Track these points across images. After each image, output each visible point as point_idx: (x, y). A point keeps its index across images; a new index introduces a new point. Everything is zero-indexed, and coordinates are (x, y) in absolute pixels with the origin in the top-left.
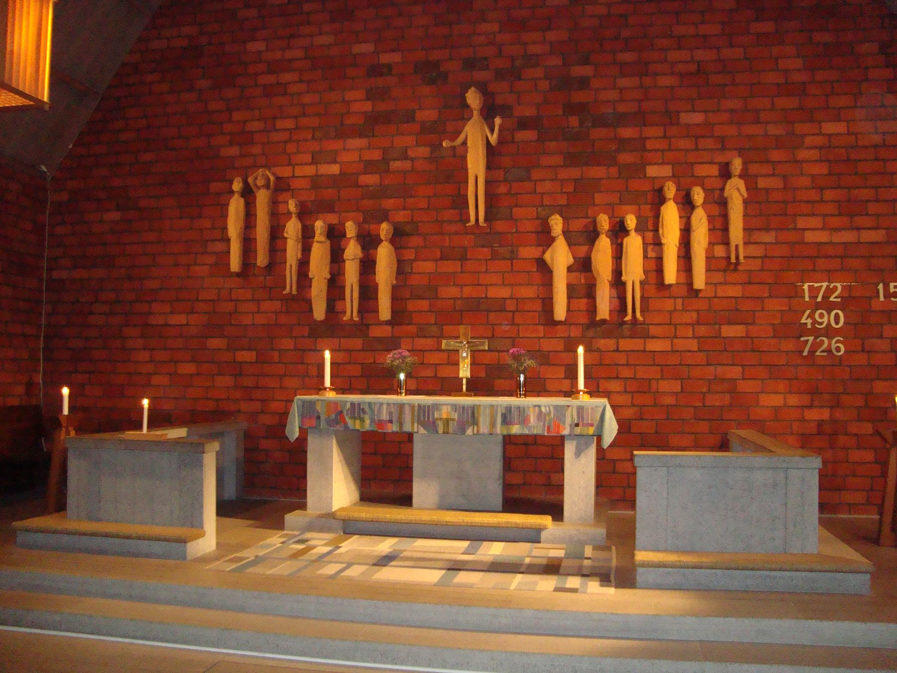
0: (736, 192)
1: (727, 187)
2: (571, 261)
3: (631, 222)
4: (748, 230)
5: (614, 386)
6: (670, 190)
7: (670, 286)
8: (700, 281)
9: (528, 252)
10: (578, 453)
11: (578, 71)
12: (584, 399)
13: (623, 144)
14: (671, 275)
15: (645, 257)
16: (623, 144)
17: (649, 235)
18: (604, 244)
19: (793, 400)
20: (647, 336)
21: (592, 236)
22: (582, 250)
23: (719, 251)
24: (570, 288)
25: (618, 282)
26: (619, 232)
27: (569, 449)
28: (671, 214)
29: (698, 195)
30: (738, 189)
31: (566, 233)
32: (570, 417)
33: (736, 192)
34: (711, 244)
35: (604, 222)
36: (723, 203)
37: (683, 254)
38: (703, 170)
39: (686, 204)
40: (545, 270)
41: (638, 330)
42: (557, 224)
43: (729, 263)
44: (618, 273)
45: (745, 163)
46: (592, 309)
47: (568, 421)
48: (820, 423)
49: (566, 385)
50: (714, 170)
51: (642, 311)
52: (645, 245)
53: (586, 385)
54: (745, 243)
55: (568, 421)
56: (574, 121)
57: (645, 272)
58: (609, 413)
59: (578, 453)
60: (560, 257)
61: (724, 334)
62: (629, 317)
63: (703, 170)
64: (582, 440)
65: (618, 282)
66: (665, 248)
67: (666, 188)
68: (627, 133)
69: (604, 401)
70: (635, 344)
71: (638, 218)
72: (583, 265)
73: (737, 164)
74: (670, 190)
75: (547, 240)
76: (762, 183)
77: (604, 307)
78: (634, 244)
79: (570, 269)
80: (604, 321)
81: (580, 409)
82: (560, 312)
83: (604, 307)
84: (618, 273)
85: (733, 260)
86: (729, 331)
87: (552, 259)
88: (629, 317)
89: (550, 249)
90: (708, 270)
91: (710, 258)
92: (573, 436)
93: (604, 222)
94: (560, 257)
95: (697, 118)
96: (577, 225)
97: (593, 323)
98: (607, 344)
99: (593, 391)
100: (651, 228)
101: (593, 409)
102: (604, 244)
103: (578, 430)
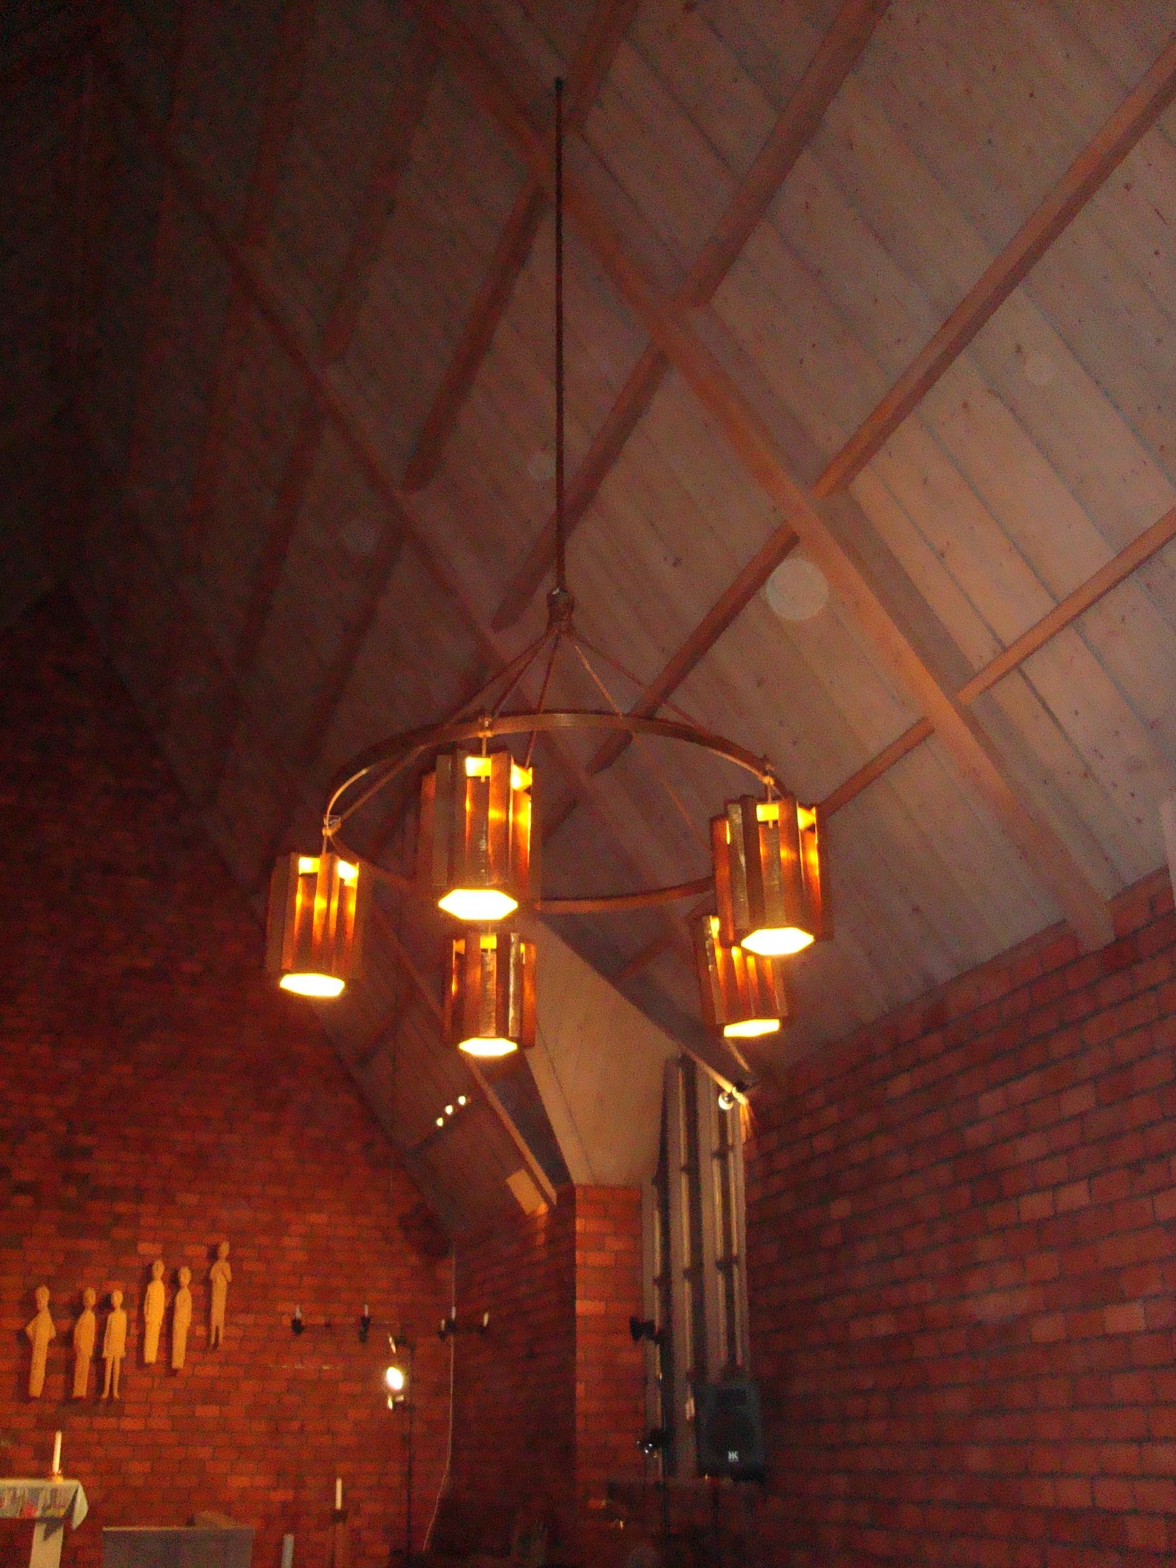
0: (221, 1275)
1: (213, 1270)
2: (54, 1334)
3: (118, 1298)
4: (228, 1311)
5: (81, 1467)
6: (159, 1269)
7: (150, 1364)
8: (178, 1361)
9: (12, 1323)
10: (47, 1535)
11: (84, 1140)
12: (59, 1481)
13: (118, 1219)
14: (151, 1353)
15: (128, 1334)
16: (118, 1219)
17: (135, 1313)
18: (89, 1319)
19: (260, 1481)
20: (120, 1414)
21: (77, 1309)
22: (65, 1324)
23: (200, 1331)
24: (49, 1363)
25: (99, 1361)
26: (104, 1307)
27: (39, 1532)
28: (157, 1293)
29: (185, 1276)
30: (223, 1273)
31: (51, 1305)
32: (44, 1498)
33: (221, 1275)
34: (193, 1323)
35: (91, 1297)
36: (208, 1283)
37: (164, 1331)
38: (191, 1250)
39: (173, 1284)
40: (26, 1344)
41: (115, 1408)
42: (43, 1296)
43: (208, 1344)
44: (99, 1346)
45: (232, 1248)
46: (70, 1384)
47: (40, 1504)
48: (285, 1505)
49: (33, 1465)
50: (203, 1251)
51: (119, 1389)
52: (129, 1322)
53: (61, 1466)
54: (226, 1325)
55: (40, 1504)
56: (71, 1192)
57: (126, 1348)
58: (81, 1490)
59: (47, 1535)
60: (43, 1329)
61: (197, 1414)
62: (105, 1395)
63: (191, 1250)
64: (52, 1524)
65: (99, 1361)
66: (148, 1327)
67: (154, 1267)
68: (122, 1207)
69: (74, 1483)
70: (112, 1422)
71: (125, 1294)
72: (65, 1340)
73: (225, 1249)
74: (159, 1269)
75: (30, 1309)
76: (247, 1266)
77: (81, 1388)
78: (118, 1320)
79: (51, 1343)
80: (80, 1399)
81: (54, 1492)
82: (36, 1388)
83: (81, 1388)
84: (99, 1346)
85: (213, 1340)
86: (201, 1411)
87: (35, 1331)
88: (105, 1395)
89: (33, 1323)
90: (189, 1348)
91: (191, 1333)
92: (42, 1520)
93: (91, 1297)
94: (43, 1329)
95: (191, 1199)
96: (65, 1297)
97: (69, 1399)
98: (80, 1422)
99: (67, 1473)
100: (137, 1305)
101: (67, 1490)
102: (89, 1319)
103: (50, 1513)
